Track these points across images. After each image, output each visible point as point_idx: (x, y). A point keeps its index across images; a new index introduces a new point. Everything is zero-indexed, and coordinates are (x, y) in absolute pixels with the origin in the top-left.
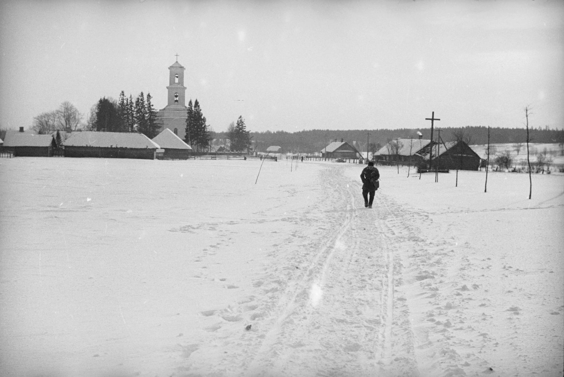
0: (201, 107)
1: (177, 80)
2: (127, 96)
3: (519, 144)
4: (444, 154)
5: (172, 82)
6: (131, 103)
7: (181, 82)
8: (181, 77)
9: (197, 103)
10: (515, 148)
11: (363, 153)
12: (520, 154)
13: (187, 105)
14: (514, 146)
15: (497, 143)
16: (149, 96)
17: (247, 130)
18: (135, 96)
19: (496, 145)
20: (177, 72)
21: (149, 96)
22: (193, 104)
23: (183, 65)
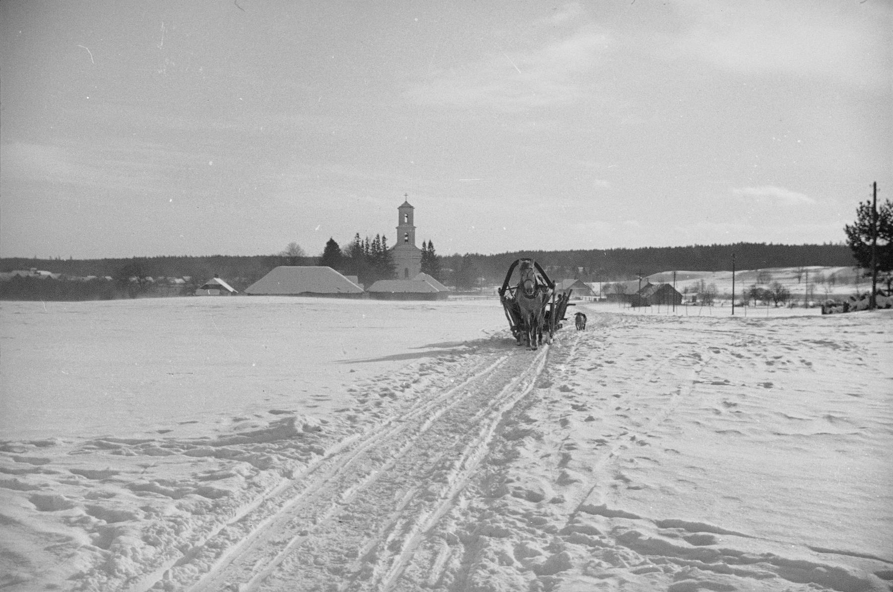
0: (435, 248)
1: (406, 220)
2: (363, 238)
3: (801, 268)
4: (73, 282)
5: (401, 221)
6: (367, 245)
7: (411, 221)
8: (410, 217)
9: (430, 244)
10: (797, 274)
11: (593, 284)
12: (721, 282)
13: (420, 247)
14: (794, 272)
15: (771, 267)
16: (384, 238)
17: (463, 255)
18: (372, 239)
19: (772, 270)
20: (406, 210)
21: (384, 238)
22: (427, 245)
23: (412, 205)
